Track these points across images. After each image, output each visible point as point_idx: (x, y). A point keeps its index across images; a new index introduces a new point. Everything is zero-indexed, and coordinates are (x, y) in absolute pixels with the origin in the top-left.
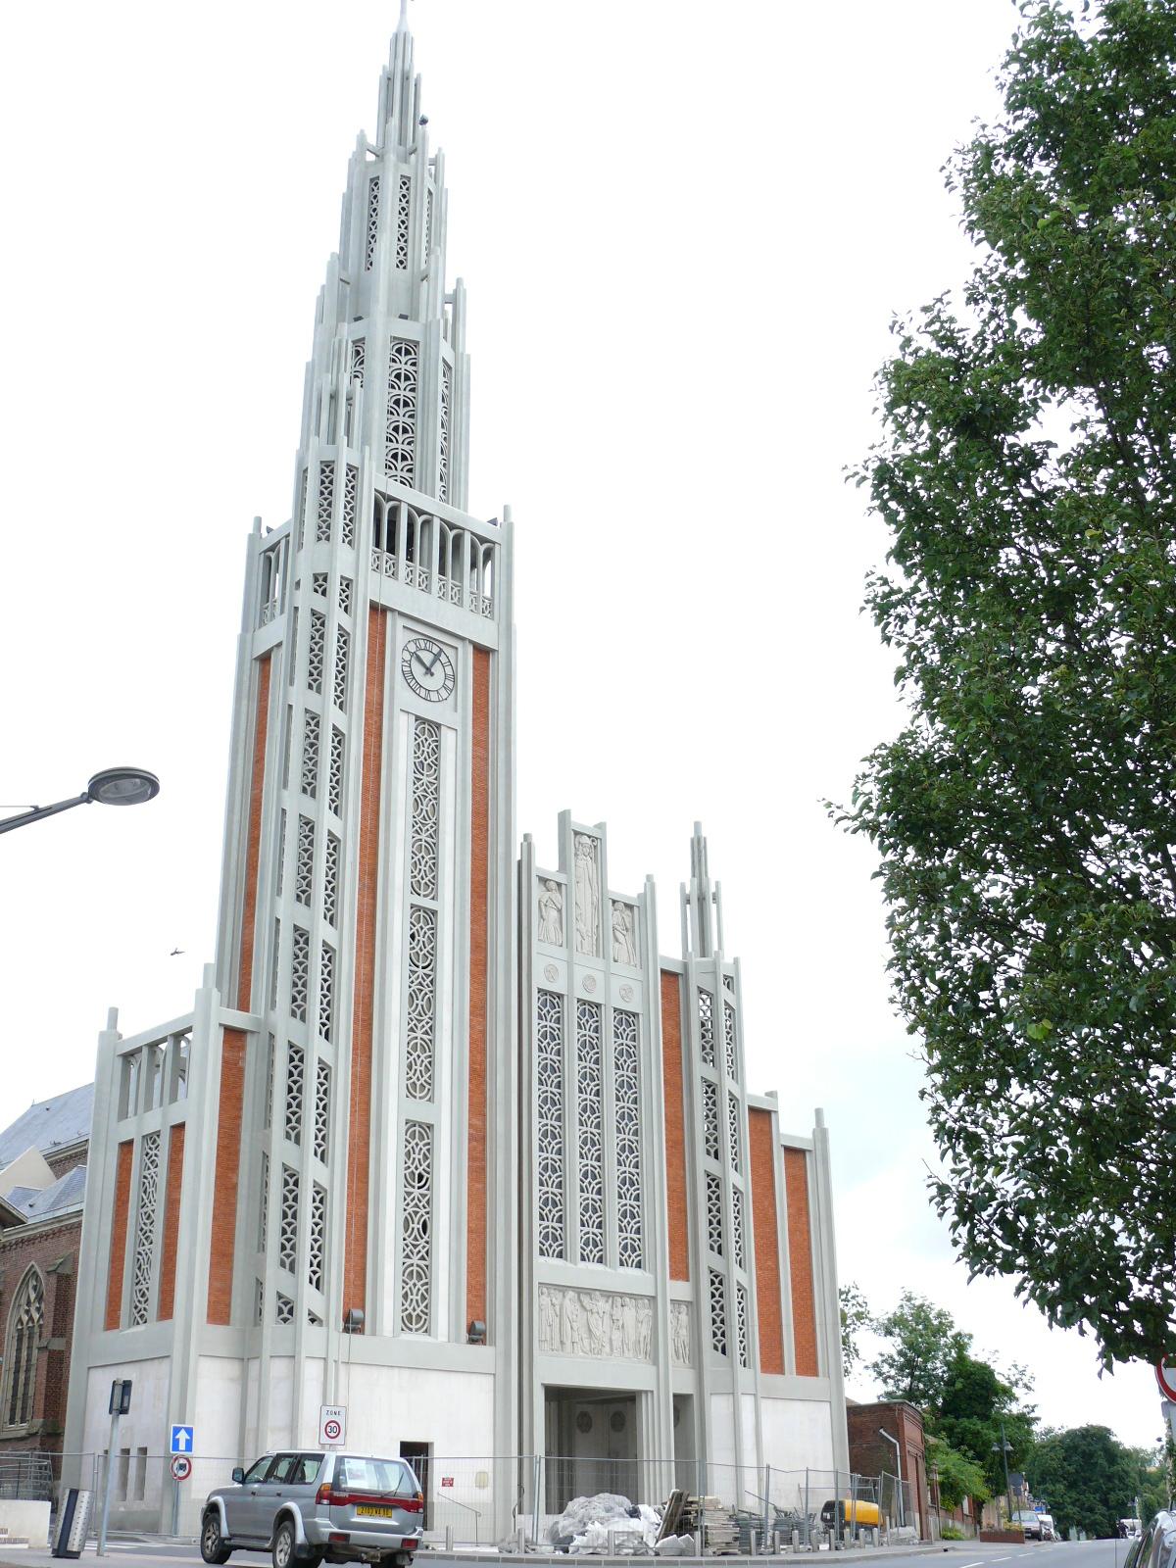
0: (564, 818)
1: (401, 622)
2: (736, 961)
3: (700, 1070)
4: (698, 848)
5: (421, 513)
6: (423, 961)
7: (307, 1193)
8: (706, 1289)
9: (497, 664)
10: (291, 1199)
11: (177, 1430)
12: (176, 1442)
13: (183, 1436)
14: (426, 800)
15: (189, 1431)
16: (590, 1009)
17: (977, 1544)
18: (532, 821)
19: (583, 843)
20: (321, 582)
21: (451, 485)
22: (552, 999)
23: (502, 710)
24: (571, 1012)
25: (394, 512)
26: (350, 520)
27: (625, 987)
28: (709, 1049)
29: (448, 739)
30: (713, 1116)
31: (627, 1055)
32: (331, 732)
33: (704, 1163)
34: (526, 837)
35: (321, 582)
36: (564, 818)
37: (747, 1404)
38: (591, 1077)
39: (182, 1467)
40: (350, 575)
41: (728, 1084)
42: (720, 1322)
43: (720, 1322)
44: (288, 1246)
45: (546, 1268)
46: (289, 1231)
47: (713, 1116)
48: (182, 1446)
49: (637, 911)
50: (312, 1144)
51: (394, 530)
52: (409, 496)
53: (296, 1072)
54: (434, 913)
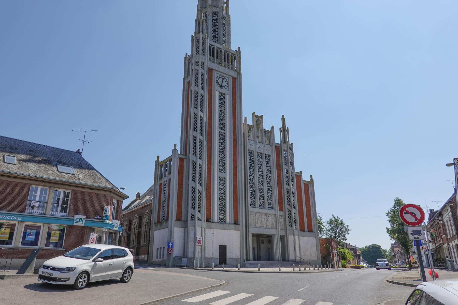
0: (254, 114)
1: (216, 72)
2: (292, 143)
3: (285, 167)
4: (283, 120)
5: (219, 49)
6: (222, 189)
7: (197, 192)
8: (287, 213)
9: (237, 81)
10: (194, 193)
11: (169, 243)
12: (169, 246)
13: (170, 244)
14: (222, 127)
15: (172, 243)
16: (260, 154)
17: (350, 269)
18: (247, 115)
19: (258, 120)
20: (197, 64)
21: (227, 41)
22: (251, 152)
23: (239, 117)
24: (256, 155)
25: (214, 48)
26: (203, 50)
27: (267, 150)
28: (286, 162)
29: (227, 97)
30: (288, 177)
31: (268, 164)
32: (199, 141)
33: (286, 186)
34: (246, 118)
35: (197, 64)
36: (254, 114)
37: (297, 237)
38: (261, 182)
39: (170, 251)
40: (203, 61)
41: (291, 169)
42: (290, 220)
43: (290, 220)
44: (193, 204)
45: (251, 209)
46: (194, 173)
47: (288, 177)
48: (170, 247)
49: (270, 134)
50: (199, 156)
51: (214, 53)
52: (217, 45)
53: (194, 167)
54: (225, 133)
